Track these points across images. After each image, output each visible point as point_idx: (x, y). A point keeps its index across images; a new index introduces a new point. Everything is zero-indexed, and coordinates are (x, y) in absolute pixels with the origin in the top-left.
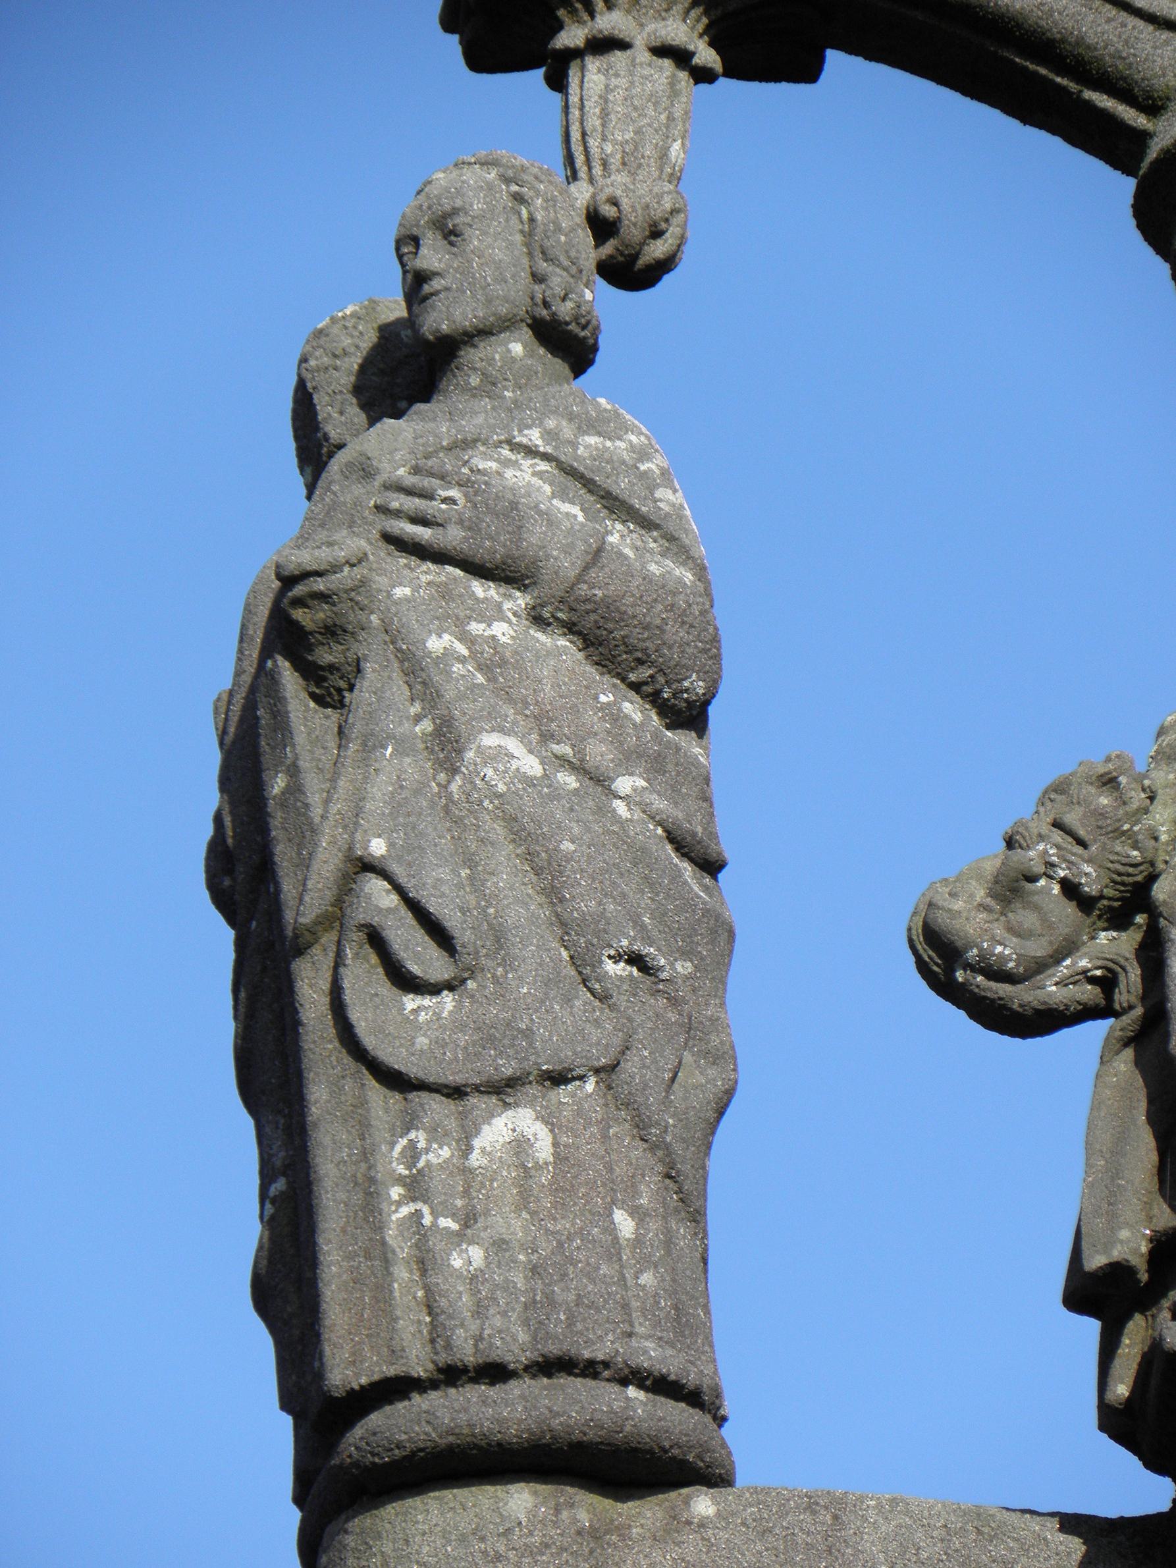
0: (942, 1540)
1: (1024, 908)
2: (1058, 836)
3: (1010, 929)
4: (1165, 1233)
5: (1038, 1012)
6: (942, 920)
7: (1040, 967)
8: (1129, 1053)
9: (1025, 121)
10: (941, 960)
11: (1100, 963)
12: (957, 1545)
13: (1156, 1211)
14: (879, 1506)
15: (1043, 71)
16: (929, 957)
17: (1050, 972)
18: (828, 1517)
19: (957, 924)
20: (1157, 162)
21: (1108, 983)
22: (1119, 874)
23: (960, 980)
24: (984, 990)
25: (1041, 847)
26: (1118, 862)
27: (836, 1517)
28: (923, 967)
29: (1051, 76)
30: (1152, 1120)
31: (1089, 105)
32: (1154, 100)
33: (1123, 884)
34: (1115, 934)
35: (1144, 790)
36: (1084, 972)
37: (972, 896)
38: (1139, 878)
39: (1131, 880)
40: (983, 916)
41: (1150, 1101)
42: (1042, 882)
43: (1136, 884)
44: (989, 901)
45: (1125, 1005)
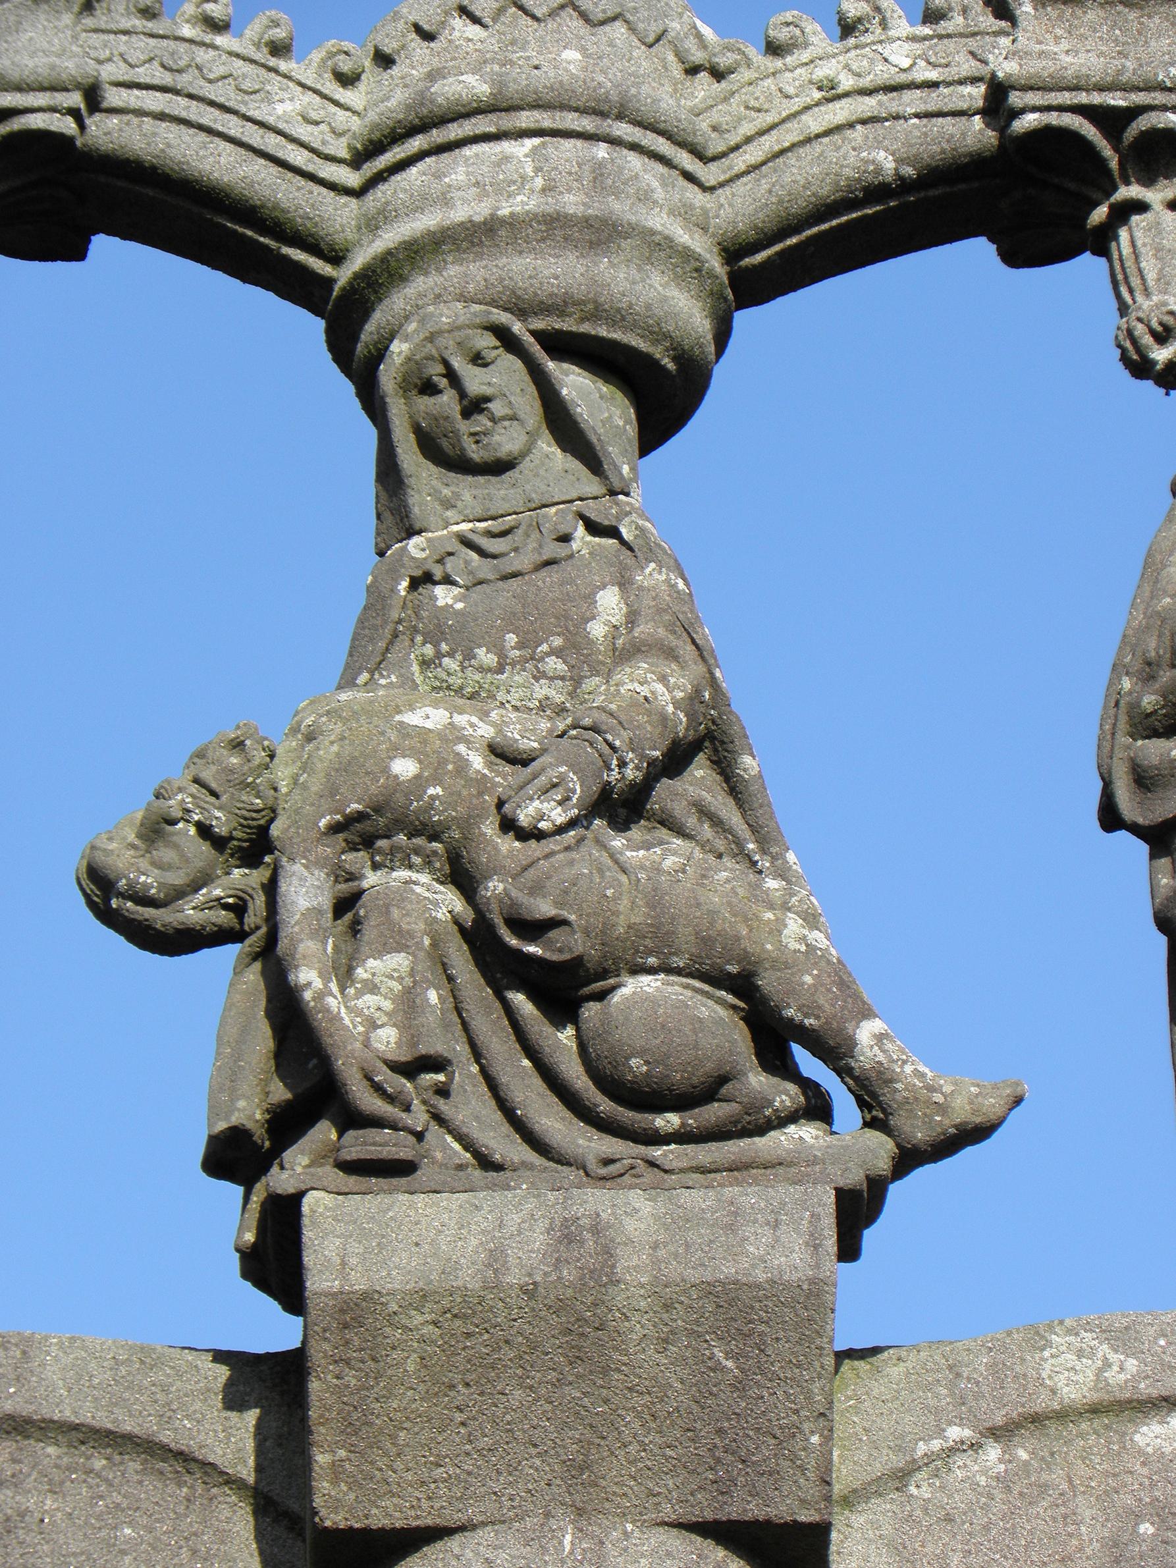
0: (111, 1369)
1: (165, 846)
2: (194, 788)
3: (153, 864)
4: (279, 1106)
5: (178, 931)
6: (100, 859)
7: (179, 893)
8: (257, 966)
9: (244, 281)
10: (102, 892)
11: (231, 892)
12: (124, 1372)
13: (272, 1088)
14: (60, 1344)
15: (249, 233)
16: (92, 890)
17: (187, 899)
18: (18, 1352)
19: (110, 860)
20: (339, 298)
21: (239, 909)
22: (246, 819)
23: (114, 906)
24: (132, 913)
25: (179, 797)
26: (244, 808)
27: (24, 1353)
28: (91, 904)
29: (256, 237)
30: (269, 1014)
31: (286, 259)
32: (336, 251)
33: (249, 827)
34: (247, 871)
35: (264, 749)
36: (219, 899)
37: (125, 838)
38: (262, 822)
39: (254, 823)
40: (132, 852)
41: (269, 1000)
42: (181, 825)
43: (260, 826)
44: (137, 842)
45: (253, 926)
